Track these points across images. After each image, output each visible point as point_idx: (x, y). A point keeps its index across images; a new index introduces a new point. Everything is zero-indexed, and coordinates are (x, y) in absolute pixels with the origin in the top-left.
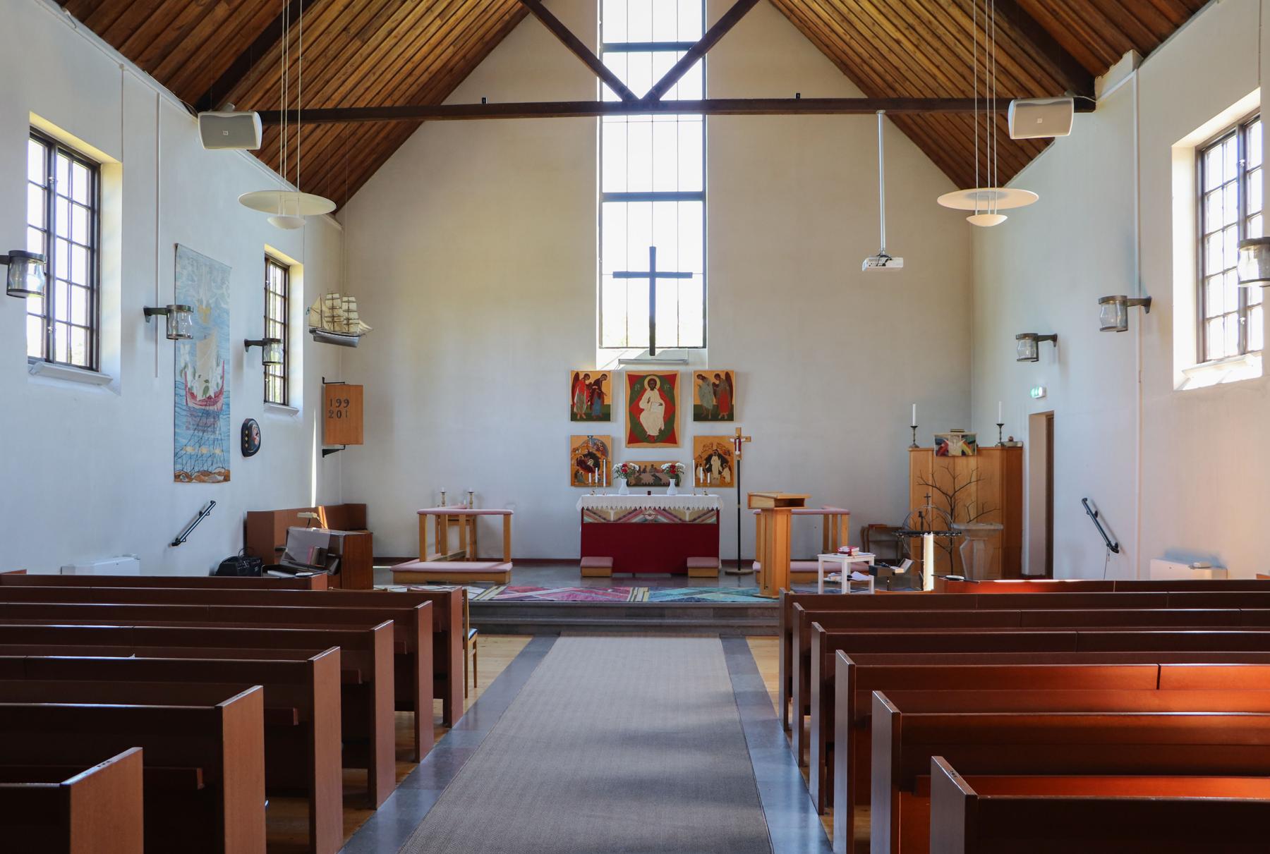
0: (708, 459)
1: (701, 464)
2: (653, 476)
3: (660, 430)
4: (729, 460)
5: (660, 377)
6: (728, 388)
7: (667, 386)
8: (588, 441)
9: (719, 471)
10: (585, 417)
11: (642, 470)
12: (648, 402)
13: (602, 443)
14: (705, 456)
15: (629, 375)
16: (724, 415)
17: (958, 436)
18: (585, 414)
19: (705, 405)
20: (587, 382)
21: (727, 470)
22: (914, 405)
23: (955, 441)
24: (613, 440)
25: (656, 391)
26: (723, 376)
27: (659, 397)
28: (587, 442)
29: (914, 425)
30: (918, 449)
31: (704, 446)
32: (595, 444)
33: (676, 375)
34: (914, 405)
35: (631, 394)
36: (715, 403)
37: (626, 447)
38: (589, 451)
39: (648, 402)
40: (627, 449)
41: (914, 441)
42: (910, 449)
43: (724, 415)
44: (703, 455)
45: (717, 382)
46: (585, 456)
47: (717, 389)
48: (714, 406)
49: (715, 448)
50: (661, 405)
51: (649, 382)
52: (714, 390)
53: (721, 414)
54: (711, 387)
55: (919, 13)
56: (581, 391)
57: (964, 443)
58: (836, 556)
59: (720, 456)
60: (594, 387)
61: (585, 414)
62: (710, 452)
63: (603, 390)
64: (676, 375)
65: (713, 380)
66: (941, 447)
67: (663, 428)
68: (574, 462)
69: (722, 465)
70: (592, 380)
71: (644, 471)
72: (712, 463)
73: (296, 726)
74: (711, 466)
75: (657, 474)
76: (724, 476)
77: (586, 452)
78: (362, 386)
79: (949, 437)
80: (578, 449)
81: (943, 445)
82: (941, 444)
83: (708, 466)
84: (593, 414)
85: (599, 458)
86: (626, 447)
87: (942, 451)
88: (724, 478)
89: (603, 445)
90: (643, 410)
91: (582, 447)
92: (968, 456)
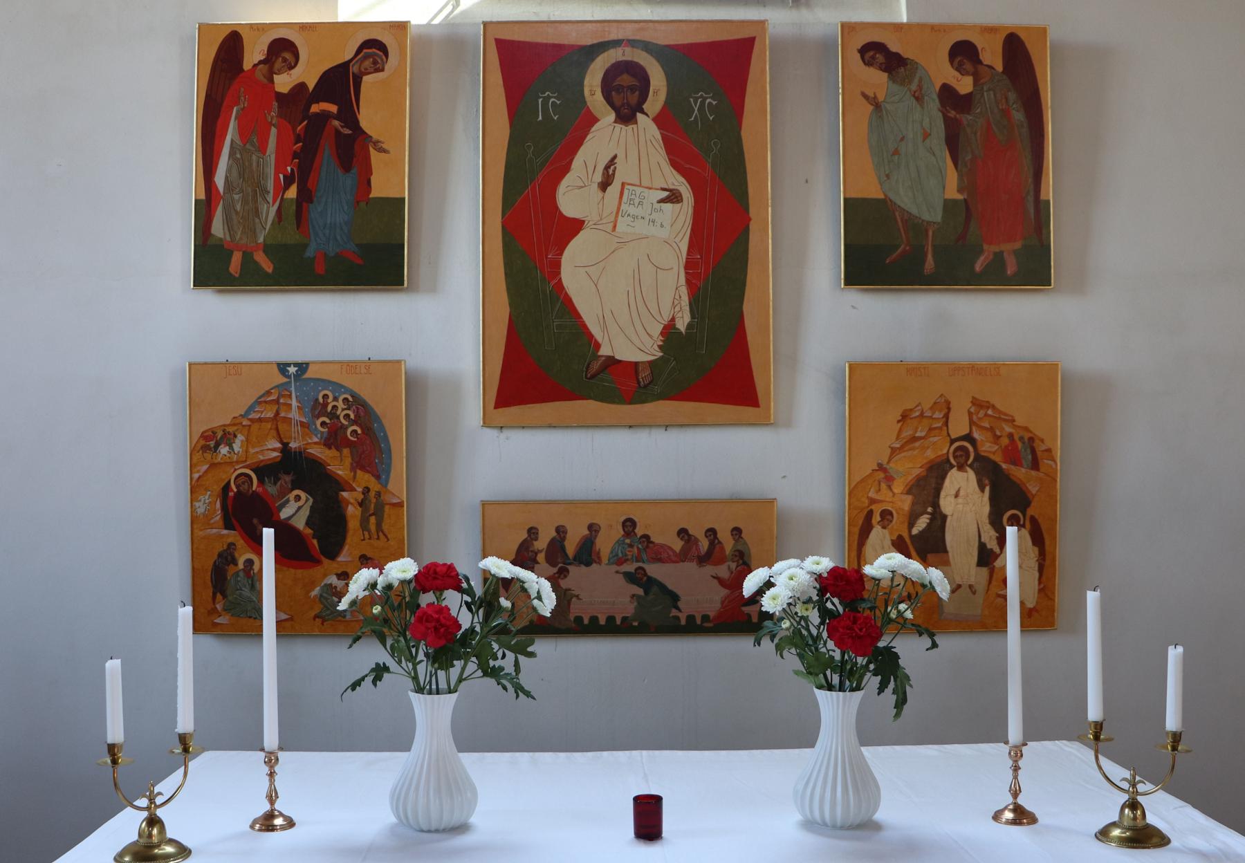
2: (631, 578)
3: (669, 330)
4: (1033, 488)
5: (665, 54)
6: (1018, 116)
7: (703, 102)
8: (283, 389)
9: (982, 547)
10: (268, 267)
11: (571, 547)
12: (604, 185)
13: (358, 403)
15: (500, 44)
16: (999, 257)
18: (268, 249)
19: (905, 200)
20: (284, 82)
24: (416, 386)
25: (645, 123)
26: (992, 56)
27: (658, 156)
28: (274, 399)
31: (905, 417)
32: (319, 408)
33: (751, 41)
35: (515, 142)
36: (952, 193)
37: (487, 423)
38: (285, 448)
39: (604, 185)
40: (491, 433)
43: (999, 257)
45: (965, 85)
46: (265, 471)
47: (966, 118)
48: (949, 205)
49: (959, 426)
50: (673, 197)
51: (609, 86)
52: (947, 120)
53: (990, 250)
54: (933, 104)
56: (252, 131)
60: (315, 108)
61: (268, 249)
62: (939, 448)
63: (364, 123)
64: (751, 41)
65: (942, 72)
67: (682, 325)
68: (209, 502)
70: (307, 72)
71: (587, 554)
72: (947, 504)
73: (339, 110)
74: (939, 520)
75: (654, 570)
77: (270, 450)
80: (227, 438)
83: (922, 523)
84: (310, 252)
85: (338, 485)
86: (487, 423)
89: (362, 410)
90: (575, 226)
91: (247, 423)
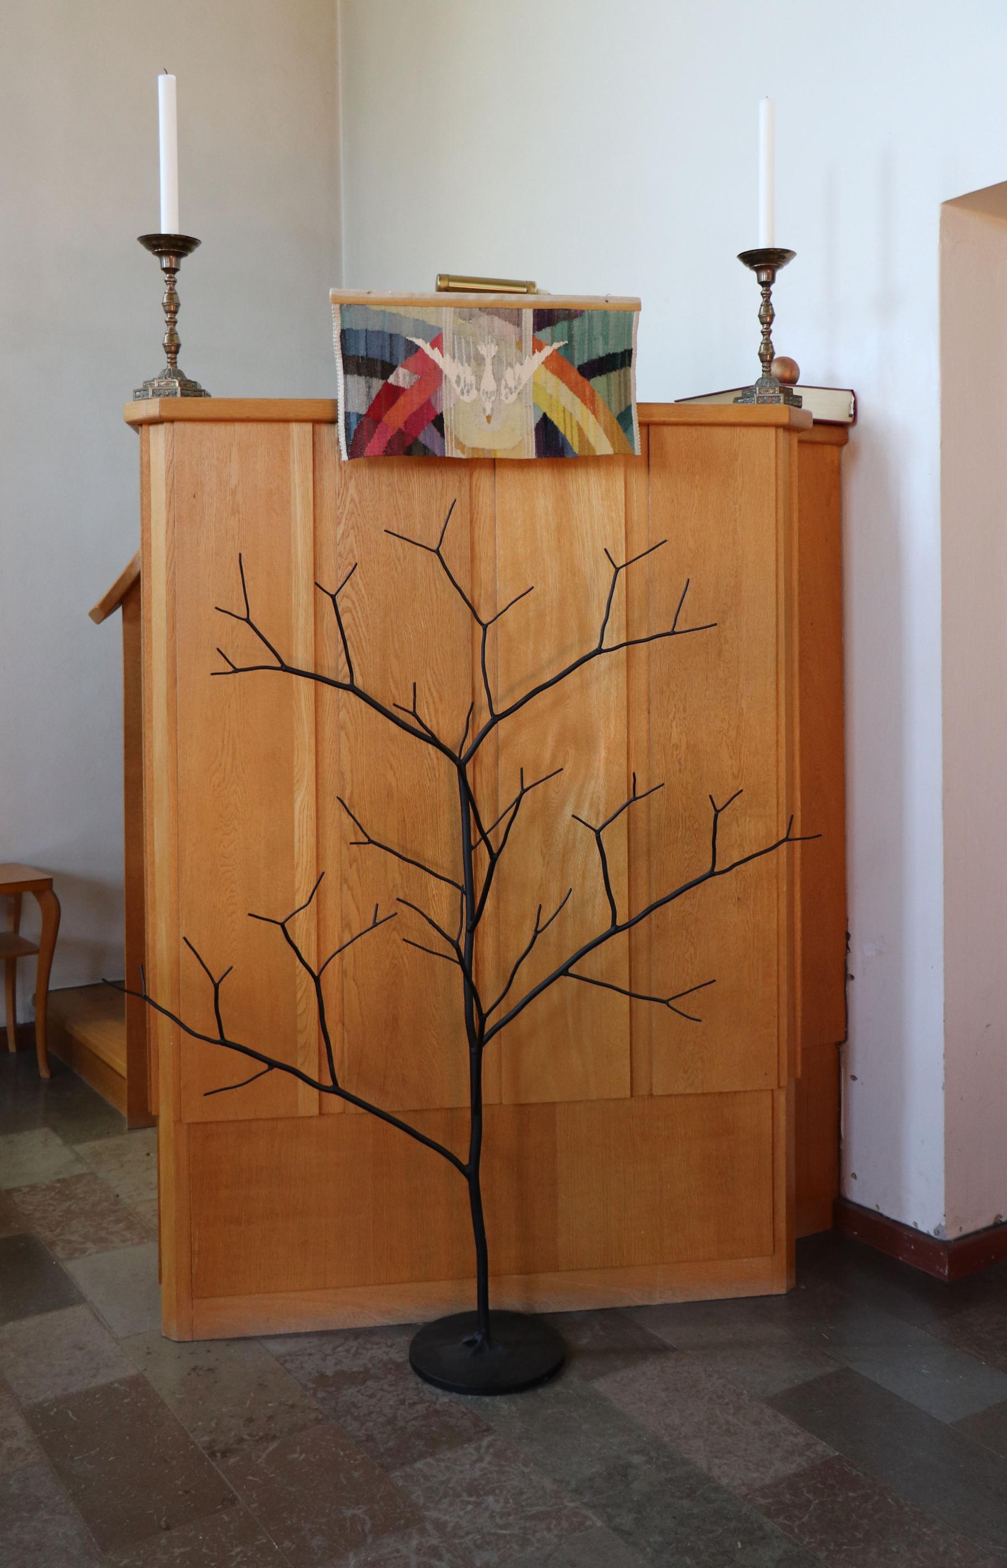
17: (514, 317)
22: (165, 85)
23: (488, 350)
29: (168, 226)
30: (192, 406)
34: (165, 85)
41: (173, 349)
42: (151, 408)
57: (557, 364)
66: (391, 394)
78: (801, 397)
79: (446, 320)
81: (401, 377)
82: (388, 368)
87: (396, 418)
92: (590, 460)
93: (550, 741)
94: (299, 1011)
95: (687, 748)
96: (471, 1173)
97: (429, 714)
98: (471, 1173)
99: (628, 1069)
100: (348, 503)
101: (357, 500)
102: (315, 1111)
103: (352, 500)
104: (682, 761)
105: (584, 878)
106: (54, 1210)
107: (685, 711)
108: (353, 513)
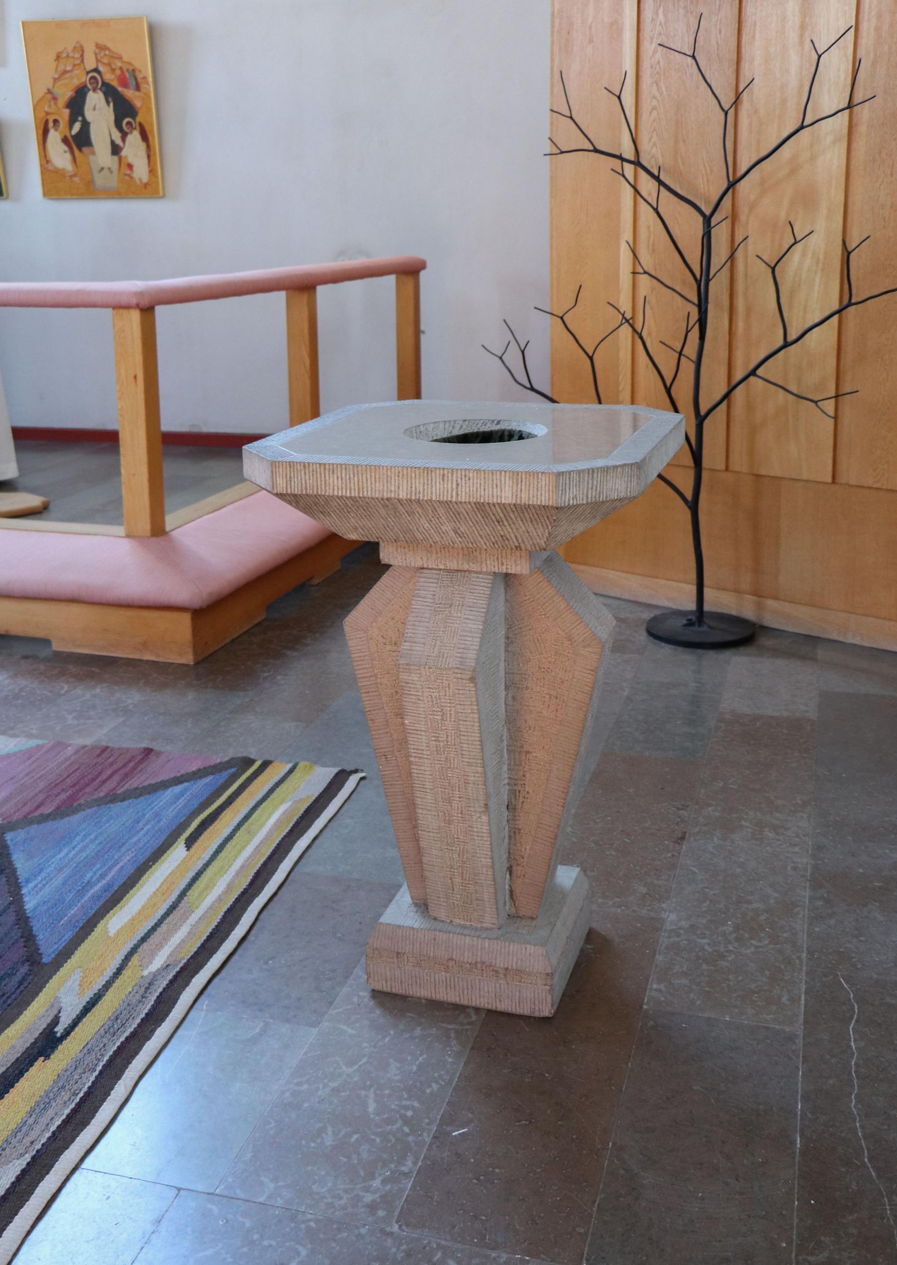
0: (76, 104)
1: (56, 122)
4: (138, 103)
9: (113, 143)
14: (65, 93)
21: (134, 137)
31: (58, 57)
44: (58, 91)
49: (90, 64)
55: (732, 131)
58: (14, 1176)
59: (110, 92)
62: (79, 78)
69: (118, 124)
72: (89, 114)
74: (86, 125)
76: (131, 160)
83: (77, 127)
88: (130, 166)
93: (786, 203)
94: (620, 388)
95: (891, 208)
96: (693, 506)
97: (703, 184)
98: (693, 506)
99: (830, 462)
100: (657, 26)
101: (663, 23)
102: (723, 467)
103: (661, 24)
104: (887, 219)
105: (805, 311)
106: (540, 686)
107: (892, 175)
108: (660, 34)
